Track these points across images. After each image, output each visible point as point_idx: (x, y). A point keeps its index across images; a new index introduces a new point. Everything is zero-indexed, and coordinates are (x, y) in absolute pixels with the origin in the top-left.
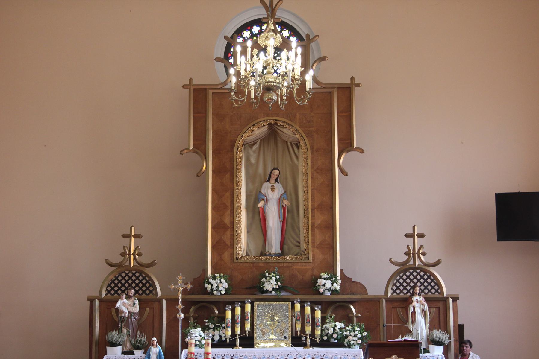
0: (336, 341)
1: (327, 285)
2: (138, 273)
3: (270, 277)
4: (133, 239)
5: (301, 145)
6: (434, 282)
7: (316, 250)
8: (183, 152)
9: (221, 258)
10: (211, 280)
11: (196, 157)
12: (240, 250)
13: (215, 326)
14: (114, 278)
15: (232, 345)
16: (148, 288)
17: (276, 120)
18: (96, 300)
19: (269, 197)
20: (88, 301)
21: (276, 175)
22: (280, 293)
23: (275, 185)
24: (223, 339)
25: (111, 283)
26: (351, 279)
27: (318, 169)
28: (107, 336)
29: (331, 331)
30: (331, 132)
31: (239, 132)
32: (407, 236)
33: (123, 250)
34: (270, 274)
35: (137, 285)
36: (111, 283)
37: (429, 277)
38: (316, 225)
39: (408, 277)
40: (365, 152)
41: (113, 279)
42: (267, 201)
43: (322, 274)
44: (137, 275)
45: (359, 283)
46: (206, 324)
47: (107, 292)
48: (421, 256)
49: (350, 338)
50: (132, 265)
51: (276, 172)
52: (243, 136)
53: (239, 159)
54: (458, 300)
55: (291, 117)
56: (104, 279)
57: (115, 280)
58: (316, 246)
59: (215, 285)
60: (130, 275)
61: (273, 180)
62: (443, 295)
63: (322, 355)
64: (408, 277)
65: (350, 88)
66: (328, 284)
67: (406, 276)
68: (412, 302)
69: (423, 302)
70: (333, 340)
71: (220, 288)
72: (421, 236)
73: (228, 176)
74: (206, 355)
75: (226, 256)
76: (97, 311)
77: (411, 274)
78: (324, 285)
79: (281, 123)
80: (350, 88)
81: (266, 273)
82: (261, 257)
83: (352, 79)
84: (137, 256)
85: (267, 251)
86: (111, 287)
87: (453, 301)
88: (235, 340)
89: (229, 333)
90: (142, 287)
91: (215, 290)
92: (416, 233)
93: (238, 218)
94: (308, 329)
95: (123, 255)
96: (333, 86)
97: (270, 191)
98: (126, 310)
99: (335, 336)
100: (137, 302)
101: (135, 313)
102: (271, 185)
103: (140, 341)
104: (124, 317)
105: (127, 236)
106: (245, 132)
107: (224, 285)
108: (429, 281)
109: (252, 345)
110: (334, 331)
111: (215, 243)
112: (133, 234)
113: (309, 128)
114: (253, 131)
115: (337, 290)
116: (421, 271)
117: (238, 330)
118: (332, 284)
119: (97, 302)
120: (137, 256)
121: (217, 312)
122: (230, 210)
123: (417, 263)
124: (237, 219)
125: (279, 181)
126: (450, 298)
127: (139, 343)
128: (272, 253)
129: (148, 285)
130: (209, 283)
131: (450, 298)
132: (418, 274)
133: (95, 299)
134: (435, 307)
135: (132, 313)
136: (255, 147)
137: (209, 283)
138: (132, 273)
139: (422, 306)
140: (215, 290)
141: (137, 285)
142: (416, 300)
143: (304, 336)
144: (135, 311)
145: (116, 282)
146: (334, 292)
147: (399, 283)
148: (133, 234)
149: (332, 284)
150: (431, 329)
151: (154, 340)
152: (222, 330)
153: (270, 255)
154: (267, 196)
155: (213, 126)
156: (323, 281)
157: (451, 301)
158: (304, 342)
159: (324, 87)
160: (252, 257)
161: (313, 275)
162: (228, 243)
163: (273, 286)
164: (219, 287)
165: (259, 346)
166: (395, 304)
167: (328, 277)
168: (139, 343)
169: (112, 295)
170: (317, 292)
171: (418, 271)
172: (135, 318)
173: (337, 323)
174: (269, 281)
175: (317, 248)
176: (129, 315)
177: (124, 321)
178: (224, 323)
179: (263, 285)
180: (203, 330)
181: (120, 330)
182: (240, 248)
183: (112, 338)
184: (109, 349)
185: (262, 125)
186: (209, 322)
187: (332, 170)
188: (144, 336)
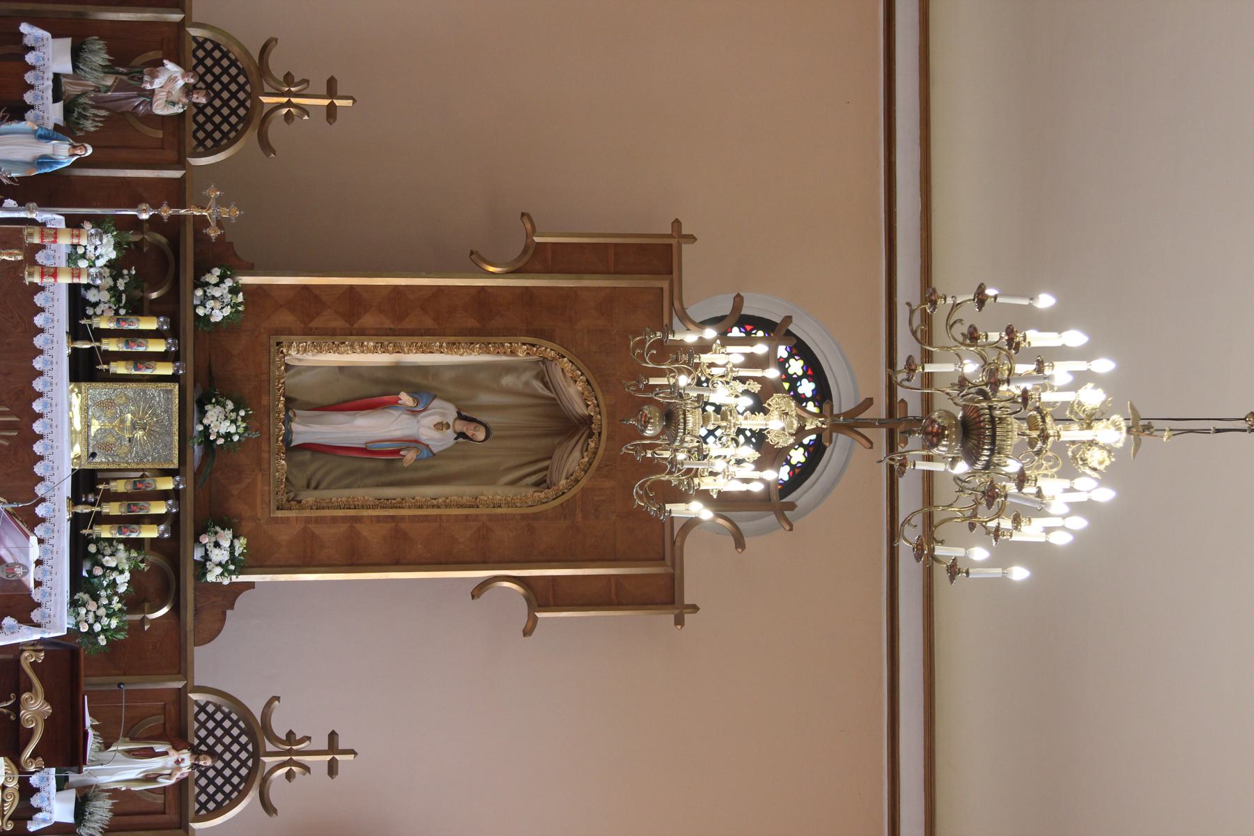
0: (85, 574)
1: (216, 551)
2: (246, 114)
4: (326, 102)
6: (223, 801)
9: (281, 306)
10: (229, 283)
14: (233, 58)
15: (76, 332)
16: (209, 135)
17: (600, 434)
22: (199, 444)
23: (450, 432)
25: (221, 50)
26: (232, 607)
28: (96, 40)
30: (571, 561)
32: (333, 736)
34: (244, 419)
35: (217, 111)
36: (221, 50)
37: (235, 787)
38: (357, 526)
39: (235, 740)
40: (526, 638)
41: (231, 55)
43: (243, 541)
44: (242, 112)
46: (125, 272)
47: (201, 40)
49: (92, 606)
50: (265, 99)
52: (564, 357)
55: (606, 469)
56: (232, 34)
57: (229, 59)
58: (309, 526)
59: (217, 292)
60: (241, 96)
64: (235, 740)
65: (672, 602)
66: (219, 555)
67: (239, 735)
68: (177, 748)
69: (178, 775)
71: (210, 304)
72: (332, 769)
74: (52, 270)
75: (286, 318)
77: (243, 747)
78: (217, 545)
79: (592, 445)
80: (672, 602)
81: (246, 411)
82: (282, 398)
83: (694, 608)
84: (285, 111)
85: (297, 412)
86: (213, 50)
90: (213, 123)
91: (205, 292)
92: (337, 757)
94: (113, 509)
95: (289, 79)
96: (677, 563)
97: (437, 419)
98: (157, 83)
100: (178, 109)
101: (151, 106)
103: (86, 118)
104: (141, 80)
107: (216, 312)
112: (338, 102)
114: (576, 381)
115: (204, 574)
116: (250, 769)
117: (112, 346)
118: (220, 564)
120: (285, 111)
121: (154, 295)
122: (392, 326)
125: (461, 440)
130: (222, 279)
132: (243, 763)
133: (183, 11)
134: (164, 803)
135: (152, 99)
136: (538, 386)
137: (222, 279)
138: (245, 100)
139: (168, 772)
140: (205, 292)
141: (217, 111)
142: (183, 760)
145: (225, 63)
146: (202, 567)
149: (220, 564)
150: (115, 793)
152: (110, 308)
153: (288, 421)
154: (424, 413)
156: (226, 544)
163: (216, 426)
164: (212, 301)
167: (237, 554)
168: (79, 113)
169: (194, 52)
170: (200, 530)
171: (250, 763)
172: (139, 105)
173: (127, 576)
174: (226, 418)
177: (132, 78)
178: (127, 313)
179: (218, 403)
181: (112, 70)
183: (91, 51)
184: (67, 43)
185: (589, 403)
186: (130, 277)
187: (484, 562)
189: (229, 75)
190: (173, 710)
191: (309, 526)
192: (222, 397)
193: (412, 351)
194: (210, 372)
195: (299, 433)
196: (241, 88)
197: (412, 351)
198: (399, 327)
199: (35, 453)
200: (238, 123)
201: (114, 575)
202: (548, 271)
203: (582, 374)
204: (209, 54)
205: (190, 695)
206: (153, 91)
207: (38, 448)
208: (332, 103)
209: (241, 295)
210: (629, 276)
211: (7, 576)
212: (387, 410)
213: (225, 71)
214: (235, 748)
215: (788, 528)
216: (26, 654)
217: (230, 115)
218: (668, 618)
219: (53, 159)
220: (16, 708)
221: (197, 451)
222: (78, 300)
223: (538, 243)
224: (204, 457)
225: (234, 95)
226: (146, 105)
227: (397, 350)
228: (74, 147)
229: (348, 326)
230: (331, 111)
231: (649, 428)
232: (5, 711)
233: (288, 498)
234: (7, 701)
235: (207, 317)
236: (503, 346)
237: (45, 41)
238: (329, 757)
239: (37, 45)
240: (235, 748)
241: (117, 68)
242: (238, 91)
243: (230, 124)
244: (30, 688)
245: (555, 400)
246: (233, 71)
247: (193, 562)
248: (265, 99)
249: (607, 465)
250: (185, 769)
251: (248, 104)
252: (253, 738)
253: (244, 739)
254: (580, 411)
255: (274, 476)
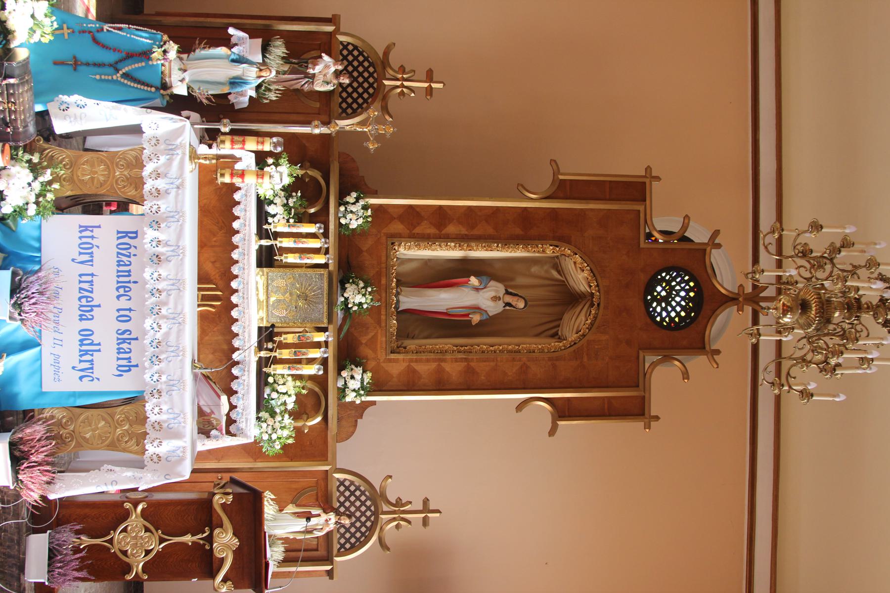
0: (266, 396)
1: (352, 381)
2: (374, 93)
3: (366, 293)
4: (426, 85)
5: (560, 342)
6: (355, 542)
7: (405, 364)
8: (553, 164)
9: (395, 218)
10: (362, 202)
11: (546, 183)
12: (405, 248)
13: (291, 208)
14: (366, 55)
15: (262, 233)
16: (350, 106)
17: (599, 305)
18: (334, 27)
19: (483, 292)
20: (333, 15)
21: (516, 304)
22: (342, 310)
23: (501, 302)
24: (270, 220)
25: (358, 51)
26: (361, 417)
27: (527, 367)
28: (278, 38)
29: (282, 389)
30: (581, 388)
31: (583, 250)
32: (426, 501)
33: (409, 70)
34: (370, 293)
35: (355, 90)
36: (358, 51)
37: (363, 534)
38: (442, 364)
39: (363, 503)
40: (550, 438)
41: (365, 53)
42: (477, 289)
43: (369, 374)
44: (371, 91)
45: (355, 431)
46: (294, 194)
47: (345, 44)
48: (395, 523)
49: (270, 421)
50: (386, 82)
51: (521, 304)
52: (576, 254)
53: (542, 248)
54: (330, 579)
55: (603, 327)
56: (366, 40)
57: (363, 56)
58: (412, 364)
59: (352, 208)
60: (371, 80)
61: (508, 299)
62: (337, 556)
63: (243, 378)
64: (363, 503)
65: (643, 414)
66: (354, 384)
67: (366, 501)
68: (326, 512)
69: (327, 530)
70: (267, 390)
71: (350, 216)
72: (425, 522)
73: (518, 231)
74: (240, 172)
75: (397, 227)
76: (317, 28)
77: (368, 508)
78: (352, 377)
79: (593, 312)
80: (643, 414)
81: (372, 288)
82: (394, 280)
83: (657, 418)
84: (399, 90)
85: (402, 288)
86: (353, 50)
87: (327, 571)
88: (268, 237)
89: (281, 228)
90: (352, 98)
91: (346, 208)
92: (429, 515)
93: (455, 246)
94: (285, 354)
95: (402, 69)
96: (647, 389)
97: (493, 294)
98: (318, 69)
99: (274, 395)
100: (330, 88)
101: (313, 84)
102: (501, 297)
103: (270, 90)
104: (307, 67)
105: (430, 77)
106: (582, 259)
107: (353, 222)
108: (358, 535)
109: (260, 265)
110: (281, 393)
111: (418, 210)
112: (434, 85)
113: (587, 355)
114: (583, 271)
115: (344, 397)
116: (373, 522)
117: (287, 243)
118: (354, 390)
119: (330, 28)
120: (399, 90)
121: (312, 211)
122: (466, 233)
123: (384, 517)
124: (453, 244)
125: (508, 308)
126: (332, 566)
127: (265, 87)
128: (400, 296)
129: (355, 106)
130: (357, 200)
131: (332, 566)
132: (368, 519)
133: (335, 25)
134: (318, 544)
135: (313, 79)
136: (555, 274)
137: (357, 200)
138: (373, 83)
139: (321, 527)
140: (346, 208)
141: (355, 90)
142: (330, 519)
143: (274, 347)
144: (316, 84)
145: (361, 59)
146: (342, 391)
147: (355, 491)
148: (434, 85)
149: (354, 390)
150: (286, 540)
151: (271, 72)
152: (284, 218)
153: (397, 294)
154: (485, 290)
155: (592, 210)
156: (358, 377)
157: (329, 568)
158: (265, 347)
159: (645, 375)
160: (395, 266)
161: (368, 360)
162: (417, 230)
163: (353, 298)
164: (351, 214)
165: (259, 276)
166: (322, 483)
167: (365, 384)
168: (265, 87)
169: (341, 51)
170: (340, 368)
171: (372, 518)
172: (305, 84)
173: (294, 398)
174: (359, 293)
175: (409, 366)
176: (310, 74)
177: (301, 66)
178: (295, 222)
179: (353, 282)
180: (284, 189)
181: (288, 61)
182: (410, 248)
183: (274, 46)
184: (259, 41)
185: (592, 284)
186: (297, 198)
187: (524, 388)
188: (277, 97)
189: (363, 66)
190: (323, 484)
191: (412, 364)
192: (357, 278)
193: (478, 249)
194: (348, 262)
195: (403, 303)
196: (371, 75)
197: (478, 249)
198: (472, 233)
199: (232, 317)
200: (368, 98)
201: (285, 398)
202: (566, 198)
203: (588, 265)
204: (350, 53)
205: (334, 475)
206: (314, 74)
207: (234, 313)
208: (430, 85)
209: (370, 210)
210: (618, 202)
211: (204, 426)
212: (459, 288)
213: (361, 64)
214: (363, 509)
215: (715, 366)
216: (217, 497)
217: (358, 98)
218: (640, 425)
219: (242, 79)
220: (210, 539)
221: (339, 314)
222: (261, 203)
223: (561, 180)
224: (344, 319)
225: (366, 80)
226: (309, 84)
227: (469, 249)
228: (261, 70)
229: (438, 232)
230: (430, 91)
231: (788, 316)
232: (201, 542)
233: (397, 345)
234: (203, 533)
235: (347, 225)
236: (537, 247)
237: (245, 40)
238: (423, 515)
239: (239, 43)
240: (363, 509)
241: (291, 60)
242: (369, 77)
243: (363, 98)
244: (221, 526)
245: (564, 282)
246: (366, 64)
247: (336, 388)
248: (386, 82)
249: (604, 325)
250: (332, 526)
251: (375, 85)
252: (375, 503)
253: (368, 503)
254: (582, 289)
255: (389, 331)
